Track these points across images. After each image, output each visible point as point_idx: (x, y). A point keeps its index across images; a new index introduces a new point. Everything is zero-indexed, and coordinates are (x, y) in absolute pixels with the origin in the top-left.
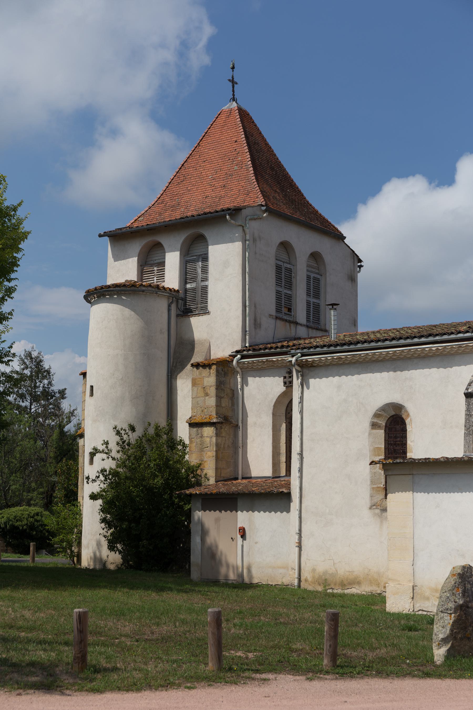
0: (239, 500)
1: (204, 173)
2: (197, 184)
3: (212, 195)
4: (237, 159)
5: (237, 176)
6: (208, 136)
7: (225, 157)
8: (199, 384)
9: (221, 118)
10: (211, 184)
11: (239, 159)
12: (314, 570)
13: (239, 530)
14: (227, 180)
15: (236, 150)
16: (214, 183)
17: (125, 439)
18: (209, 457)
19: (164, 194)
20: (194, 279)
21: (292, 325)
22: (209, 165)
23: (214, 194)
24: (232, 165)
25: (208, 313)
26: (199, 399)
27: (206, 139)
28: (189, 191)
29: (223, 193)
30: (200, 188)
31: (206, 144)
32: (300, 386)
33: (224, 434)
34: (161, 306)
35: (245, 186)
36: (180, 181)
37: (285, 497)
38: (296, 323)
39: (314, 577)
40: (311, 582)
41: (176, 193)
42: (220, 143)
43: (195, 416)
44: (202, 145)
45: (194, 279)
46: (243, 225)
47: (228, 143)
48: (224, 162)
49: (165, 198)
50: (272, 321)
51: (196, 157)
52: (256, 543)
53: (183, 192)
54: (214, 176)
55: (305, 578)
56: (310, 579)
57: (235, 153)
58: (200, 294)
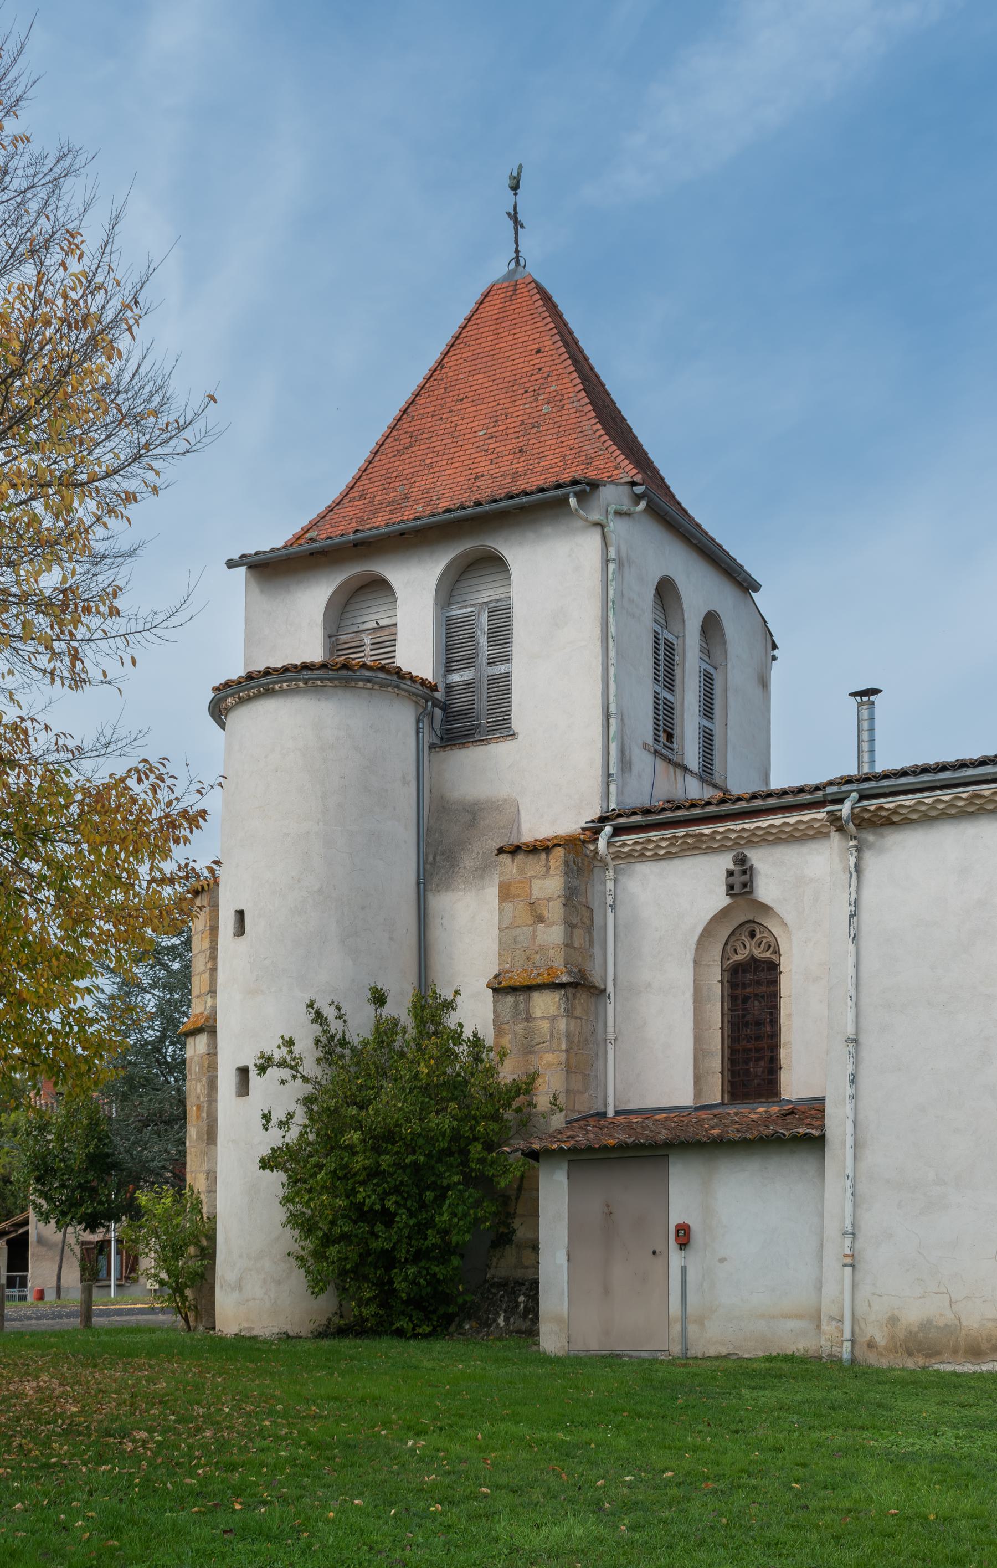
0: (671, 1159)
1: (465, 426)
2: (447, 451)
3: (491, 472)
4: (547, 390)
5: (551, 426)
6: (462, 346)
7: (515, 388)
8: (518, 896)
9: (492, 303)
10: (486, 447)
11: (552, 389)
12: (893, 1320)
13: (677, 1231)
14: (525, 438)
15: (540, 369)
16: (492, 446)
17: (333, 1031)
18: (549, 1065)
19: (364, 477)
20: (470, 661)
21: (678, 771)
22: (474, 408)
23: (497, 471)
24: (534, 404)
25: (514, 735)
26: (518, 931)
27: (457, 352)
28: (430, 466)
29: (521, 465)
30: (456, 460)
31: (461, 361)
32: (854, 874)
33: (578, 1012)
34: (398, 723)
35: (576, 446)
36: (400, 447)
37: (815, 1143)
38: (686, 769)
39: (892, 1337)
40: (886, 1349)
41: (394, 474)
42: (495, 357)
43: (508, 972)
44: (449, 365)
45: (470, 661)
46: (604, 522)
47: (517, 356)
48: (513, 399)
49: (366, 487)
50: (649, 758)
51: (436, 393)
52: (722, 1260)
53: (412, 470)
54: (490, 431)
55: (868, 1338)
56: (881, 1340)
57: (539, 376)
58: (486, 695)
